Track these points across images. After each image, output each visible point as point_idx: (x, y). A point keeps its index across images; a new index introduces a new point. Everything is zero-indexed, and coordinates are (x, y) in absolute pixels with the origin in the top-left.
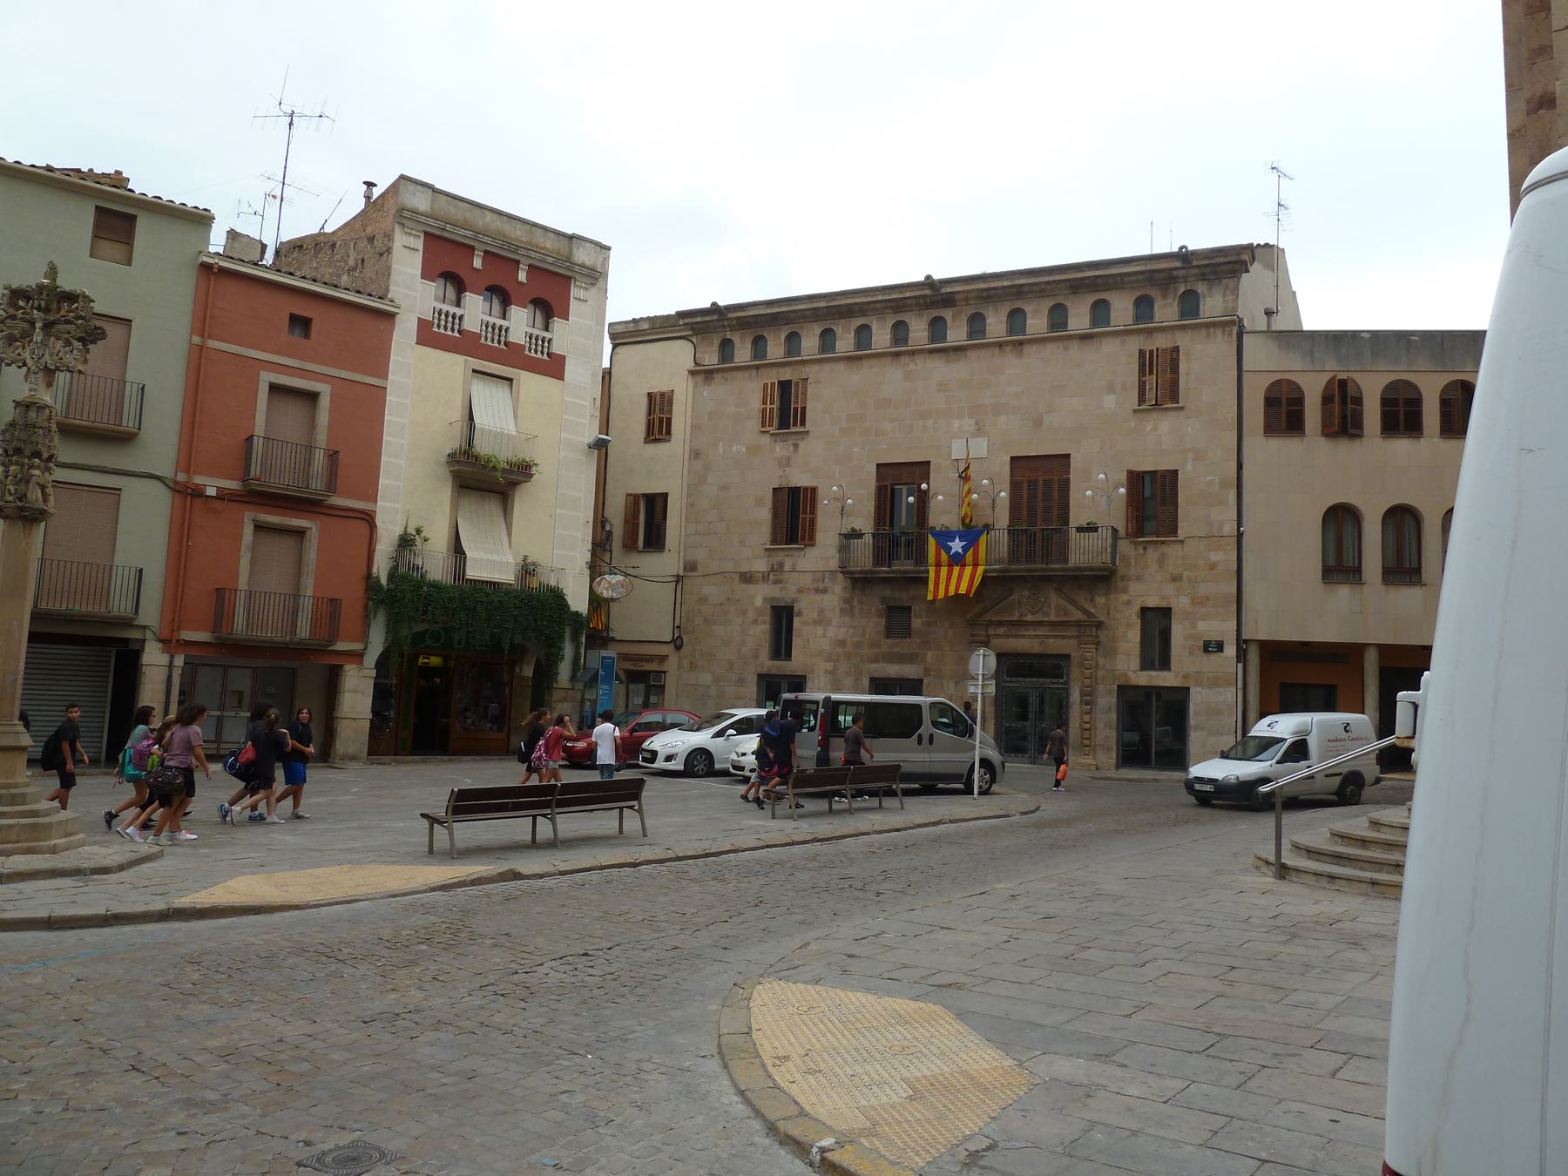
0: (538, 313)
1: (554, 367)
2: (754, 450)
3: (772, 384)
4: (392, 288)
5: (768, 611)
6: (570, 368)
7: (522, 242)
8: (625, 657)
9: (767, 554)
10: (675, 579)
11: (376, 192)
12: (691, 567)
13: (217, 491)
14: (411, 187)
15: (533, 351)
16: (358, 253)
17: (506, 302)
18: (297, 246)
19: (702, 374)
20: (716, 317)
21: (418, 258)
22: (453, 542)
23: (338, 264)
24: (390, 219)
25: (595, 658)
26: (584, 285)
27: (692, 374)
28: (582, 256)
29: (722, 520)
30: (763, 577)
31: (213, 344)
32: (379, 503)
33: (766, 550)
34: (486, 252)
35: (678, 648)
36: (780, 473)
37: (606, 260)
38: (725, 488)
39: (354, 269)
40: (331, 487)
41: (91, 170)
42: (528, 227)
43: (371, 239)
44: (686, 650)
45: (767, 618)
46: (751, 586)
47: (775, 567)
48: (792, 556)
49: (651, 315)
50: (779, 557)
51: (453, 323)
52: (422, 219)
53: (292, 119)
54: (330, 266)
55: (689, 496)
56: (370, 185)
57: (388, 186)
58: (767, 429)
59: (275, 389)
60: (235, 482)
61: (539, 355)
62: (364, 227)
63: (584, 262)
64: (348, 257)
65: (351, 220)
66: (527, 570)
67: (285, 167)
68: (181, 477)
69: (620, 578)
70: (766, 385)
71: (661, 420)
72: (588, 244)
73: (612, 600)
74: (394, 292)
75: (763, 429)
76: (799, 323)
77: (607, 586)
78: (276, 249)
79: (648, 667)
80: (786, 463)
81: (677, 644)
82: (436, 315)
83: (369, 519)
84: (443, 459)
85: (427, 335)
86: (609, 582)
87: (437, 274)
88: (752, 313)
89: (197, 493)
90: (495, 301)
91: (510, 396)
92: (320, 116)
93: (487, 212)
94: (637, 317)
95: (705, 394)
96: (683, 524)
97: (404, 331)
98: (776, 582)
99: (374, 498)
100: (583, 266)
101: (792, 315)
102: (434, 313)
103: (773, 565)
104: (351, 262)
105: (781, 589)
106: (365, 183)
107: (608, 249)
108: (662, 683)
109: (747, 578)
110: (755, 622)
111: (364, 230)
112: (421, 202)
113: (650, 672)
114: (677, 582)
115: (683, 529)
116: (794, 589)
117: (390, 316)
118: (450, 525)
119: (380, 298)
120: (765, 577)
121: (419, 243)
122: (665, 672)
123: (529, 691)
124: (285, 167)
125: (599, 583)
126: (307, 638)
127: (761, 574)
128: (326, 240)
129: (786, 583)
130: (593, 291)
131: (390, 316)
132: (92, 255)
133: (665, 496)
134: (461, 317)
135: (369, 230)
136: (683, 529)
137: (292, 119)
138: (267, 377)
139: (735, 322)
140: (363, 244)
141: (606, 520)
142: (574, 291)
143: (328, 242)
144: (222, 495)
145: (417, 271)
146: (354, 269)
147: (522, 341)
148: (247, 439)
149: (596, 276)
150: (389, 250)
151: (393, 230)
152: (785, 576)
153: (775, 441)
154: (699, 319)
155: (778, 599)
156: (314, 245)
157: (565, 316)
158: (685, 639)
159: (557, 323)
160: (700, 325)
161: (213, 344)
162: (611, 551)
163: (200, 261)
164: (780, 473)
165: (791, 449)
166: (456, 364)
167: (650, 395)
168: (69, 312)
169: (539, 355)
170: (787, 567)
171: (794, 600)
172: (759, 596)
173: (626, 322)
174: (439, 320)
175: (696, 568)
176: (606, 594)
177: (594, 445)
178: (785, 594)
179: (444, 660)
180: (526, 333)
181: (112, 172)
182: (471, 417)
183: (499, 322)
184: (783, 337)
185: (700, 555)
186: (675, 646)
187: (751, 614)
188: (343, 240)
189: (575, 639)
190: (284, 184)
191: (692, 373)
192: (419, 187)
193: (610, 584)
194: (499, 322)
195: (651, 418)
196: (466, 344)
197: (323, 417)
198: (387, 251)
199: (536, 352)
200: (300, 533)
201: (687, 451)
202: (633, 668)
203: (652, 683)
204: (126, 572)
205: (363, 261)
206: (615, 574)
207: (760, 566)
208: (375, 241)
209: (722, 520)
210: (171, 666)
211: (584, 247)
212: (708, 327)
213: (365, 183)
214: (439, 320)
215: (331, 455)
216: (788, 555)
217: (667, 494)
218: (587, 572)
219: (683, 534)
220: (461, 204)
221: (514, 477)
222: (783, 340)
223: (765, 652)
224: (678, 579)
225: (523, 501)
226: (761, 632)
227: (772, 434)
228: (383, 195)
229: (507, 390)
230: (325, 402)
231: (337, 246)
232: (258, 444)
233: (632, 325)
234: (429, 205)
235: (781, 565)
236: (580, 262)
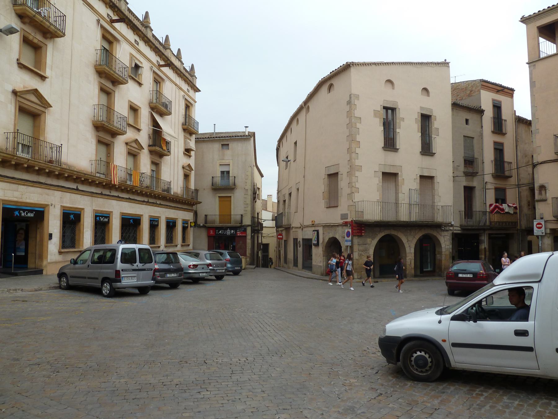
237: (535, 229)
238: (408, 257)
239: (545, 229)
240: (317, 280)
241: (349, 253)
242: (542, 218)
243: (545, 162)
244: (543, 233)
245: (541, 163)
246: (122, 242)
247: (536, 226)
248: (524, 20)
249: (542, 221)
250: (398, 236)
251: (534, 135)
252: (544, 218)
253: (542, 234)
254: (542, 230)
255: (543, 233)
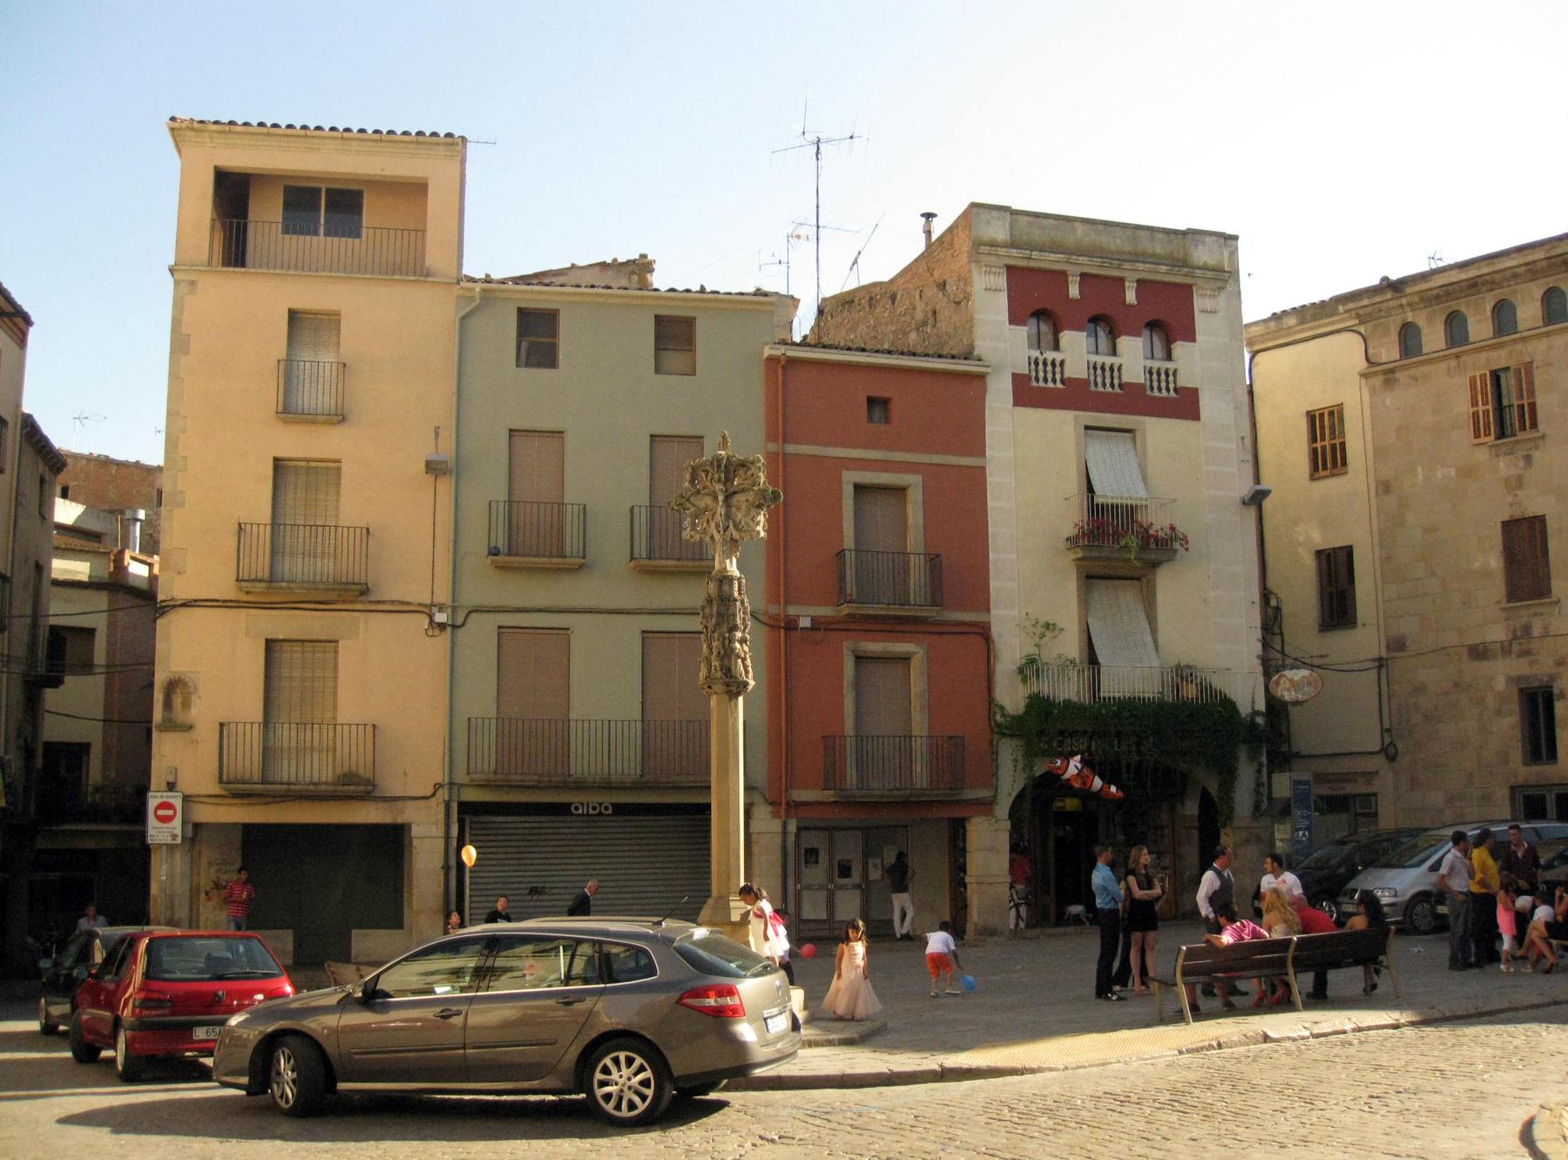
0: (1156, 339)
1: (1185, 405)
2: (1467, 472)
3: (1483, 377)
4: (977, 343)
5: (1515, 696)
6: (1206, 403)
7: (1124, 253)
8: (1320, 778)
9: (1504, 615)
10: (1377, 664)
11: (939, 228)
12: (1397, 645)
13: (812, 620)
14: (985, 215)
15: (1156, 390)
16: (927, 304)
17: (1113, 335)
18: (846, 301)
19: (1378, 374)
20: (1389, 296)
21: (1002, 300)
22: (1086, 648)
23: (903, 319)
24: (964, 259)
25: (1282, 785)
26: (1209, 292)
27: (1366, 378)
28: (1203, 255)
29: (1433, 574)
30: (1503, 648)
31: (792, 448)
32: (993, 611)
33: (1503, 609)
34: (1083, 276)
35: (1392, 759)
36: (1510, 499)
37: (1234, 253)
38: (1431, 530)
39: (924, 324)
40: (936, 599)
41: (615, 260)
42: (1129, 232)
43: (942, 286)
44: (1404, 761)
45: (1514, 707)
46: (1486, 664)
47: (1519, 633)
48: (1541, 614)
49: (1296, 305)
50: (1523, 616)
51: (1054, 373)
52: (1002, 251)
53: (818, 148)
54: (892, 322)
55: (1381, 546)
56: (929, 216)
57: (955, 218)
58: (1483, 439)
59: (859, 488)
60: (829, 608)
61: (1164, 393)
62: (931, 271)
63: (1205, 263)
64: (914, 308)
65: (912, 263)
66: (1183, 673)
67: (818, 207)
68: (774, 610)
69: (1304, 673)
70: (1473, 381)
71: (1333, 447)
72: (1208, 239)
73: (1297, 703)
74: (982, 347)
75: (1477, 441)
76: (1509, 286)
77: (1287, 685)
78: (819, 307)
79: (1350, 789)
80: (1516, 484)
81: (1389, 754)
82: (1033, 366)
83: (983, 632)
84: (1063, 545)
85: (1026, 393)
86: (1290, 680)
87: (1029, 313)
88: (1440, 283)
89: (791, 626)
90: (1102, 334)
91: (1134, 453)
92: (851, 137)
93: (1077, 224)
94: (1278, 310)
95: (1388, 402)
96: (1380, 586)
97: (999, 392)
98: (1526, 653)
99: (986, 608)
100: (1205, 268)
101: (1497, 277)
102: (1030, 363)
103: (1515, 631)
104: (919, 315)
105: (1531, 664)
106: (923, 215)
107: (1235, 238)
108: (1373, 810)
109: (1479, 652)
110: (1499, 713)
111: (932, 275)
112: (998, 231)
113: (1355, 796)
114: (1380, 667)
115: (1380, 593)
116: (1550, 661)
117: (981, 377)
118: (1080, 629)
119: (965, 359)
120: (1506, 649)
121: (1002, 281)
122: (1375, 795)
123: (1195, 833)
124: (818, 207)
125: (1277, 683)
126: (925, 785)
127: (1499, 645)
128: (883, 291)
129: (1539, 653)
130: (1222, 299)
131: (981, 377)
132: (658, 371)
133: (1349, 551)
134: (1062, 363)
135: (937, 274)
136: (1380, 593)
137: (818, 148)
138: (851, 477)
139: (1416, 299)
140: (931, 292)
141: (1271, 593)
142: (1198, 303)
143: (886, 293)
144: (818, 625)
145: (1004, 317)
146: (924, 324)
147: (1139, 378)
148: (837, 555)
149: (1225, 277)
150: (967, 297)
151: (970, 271)
152: (1535, 645)
153: (1497, 456)
154: (1365, 302)
155: (1528, 678)
156: (867, 298)
157: (1190, 336)
158: (1400, 745)
159: (1179, 348)
160: (1369, 310)
161: (792, 448)
162: (1281, 634)
163: (766, 355)
164: (1510, 499)
165: (1522, 463)
166: (1063, 424)
167: (1311, 416)
168: (745, 479)
169: (1164, 393)
170: (1536, 631)
171: (1552, 677)
172: (1501, 674)
173: (1265, 321)
174: (1037, 372)
175: (1404, 645)
176: (1287, 697)
177: (1251, 499)
178: (1540, 668)
179: (1083, 804)
180: (1145, 367)
181: (637, 257)
182: (1090, 489)
183: (1109, 360)
184: (1489, 308)
185: (1407, 627)
186: (1387, 757)
187: (1491, 702)
188: (904, 289)
189: (1253, 756)
190: (818, 227)
191: (1364, 375)
192: (995, 214)
193: (1293, 683)
194: (1109, 360)
195: (1319, 445)
196: (1073, 395)
197: (915, 513)
198: (965, 298)
199: (1160, 389)
200: (905, 659)
201: (1373, 486)
202: (1329, 792)
203: (1359, 811)
204: (593, 726)
205: (935, 313)
206: (1299, 668)
207: (1496, 633)
208: (947, 287)
209: (1433, 574)
210: (785, 833)
211: (1203, 242)
212: (1380, 311)
213: (923, 215)
214: (1037, 372)
215: (932, 560)
216: (1535, 615)
217: (1351, 547)
218: (1259, 669)
219: (1380, 600)
220: (1045, 222)
221: (1153, 557)
222: (1489, 313)
223: (1517, 754)
224: (1381, 663)
225: (1168, 584)
226: (1508, 726)
227: (1491, 446)
228: (950, 230)
229: (1129, 445)
230: (915, 497)
231: (899, 296)
232: (850, 557)
233: (1272, 324)
234: (1008, 233)
235: (1527, 629)
236: (1201, 264)
237: (152, 822)
238: (835, 1013)
239: (184, 823)
240: (456, 363)
241: (1469, 834)
242: (171, 786)
243: (198, 603)
244: (174, 837)
245: (184, 605)
246: (1333, 976)
247: (175, 813)
248: (182, 131)
249: (174, 797)
250: (1469, 321)
251: (168, 508)
252: (179, 787)
253: (174, 839)
254: (174, 828)
255: (174, 837)
